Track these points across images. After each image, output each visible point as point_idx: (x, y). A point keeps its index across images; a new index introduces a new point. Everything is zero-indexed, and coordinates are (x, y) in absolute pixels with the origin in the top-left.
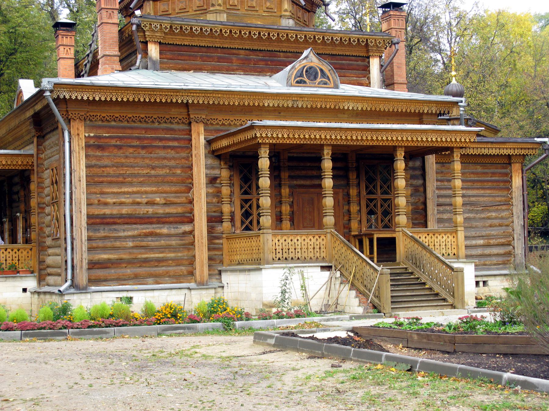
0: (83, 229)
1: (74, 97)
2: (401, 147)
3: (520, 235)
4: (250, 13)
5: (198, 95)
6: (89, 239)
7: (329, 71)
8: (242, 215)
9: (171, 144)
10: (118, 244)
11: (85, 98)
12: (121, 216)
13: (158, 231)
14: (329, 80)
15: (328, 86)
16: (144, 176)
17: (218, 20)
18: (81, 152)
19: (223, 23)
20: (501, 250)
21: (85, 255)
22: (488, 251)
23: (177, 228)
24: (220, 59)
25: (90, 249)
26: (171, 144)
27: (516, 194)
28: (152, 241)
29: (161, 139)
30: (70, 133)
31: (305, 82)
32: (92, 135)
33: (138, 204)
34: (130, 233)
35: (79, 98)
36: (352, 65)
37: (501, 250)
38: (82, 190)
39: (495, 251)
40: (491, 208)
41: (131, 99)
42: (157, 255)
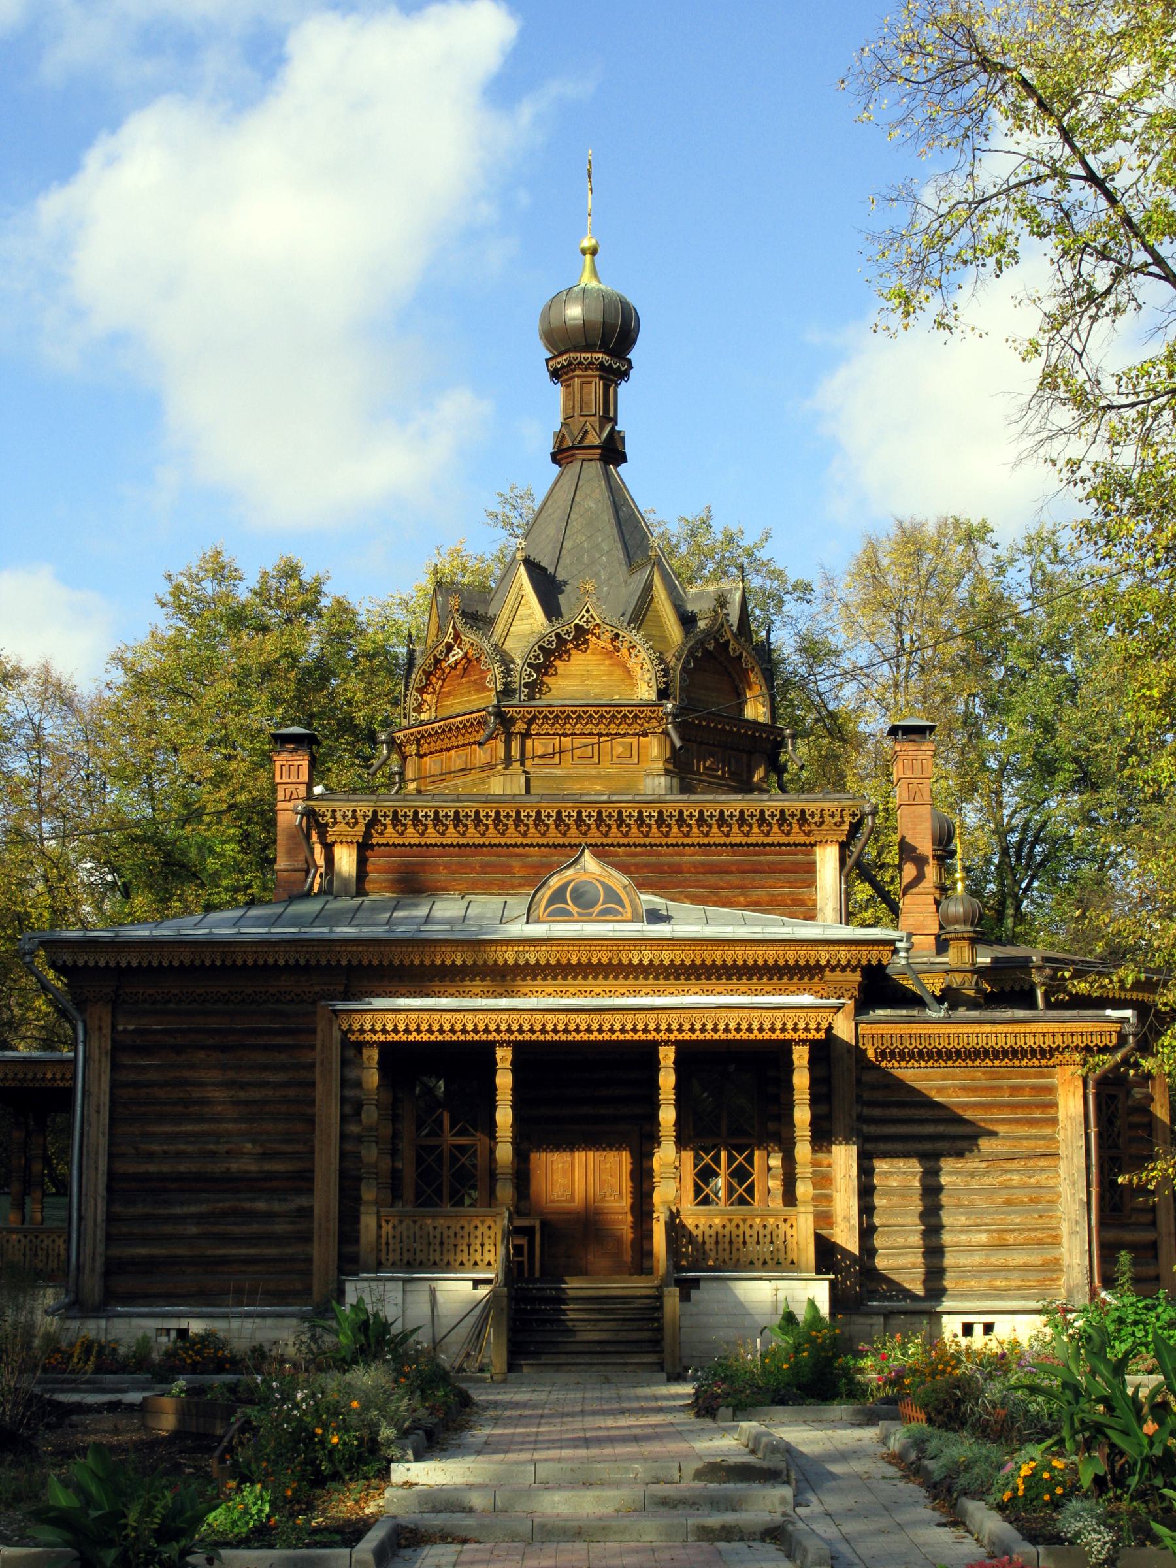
0: (99, 1199)
1: (81, 963)
2: (667, 1043)
3: (1077, 1222)
4: (581, 769)
5: (315, 949)
6: (111, 1218)
7: (625, 887)
8: (696, 1175)
9: (279, 1040)
10: (168, 1229)
11: (102, 963)
12: (180, 1177)
13: (247, 1205)
14: (623, 907)
15: (619, 918)
16: (225, 1103)
17: (508, 792)
18: (103, 1059)
19: (517, 798)
20: (1035, 1258)
21: (101, 1248)
22: (998, 1259)
23: (285, 1200)
24: (485, 868)
25: (109, 1238)
26: (279, 1040)
27: (1069, 1133)
28: (236, 1224)
29: (258, 1032)
30: (84, 1022)
31: (569, 913)
32: (131, 1027)
33: (213, 1154)
34: (193, 1209)
35: (91, 963)
36: (781, 862)
37: (1035, 1258)
38: (101, 1129)
39: (1019, 1258)
40: (1008, 1165)
41: (134, 963)
42: (244, 1251)
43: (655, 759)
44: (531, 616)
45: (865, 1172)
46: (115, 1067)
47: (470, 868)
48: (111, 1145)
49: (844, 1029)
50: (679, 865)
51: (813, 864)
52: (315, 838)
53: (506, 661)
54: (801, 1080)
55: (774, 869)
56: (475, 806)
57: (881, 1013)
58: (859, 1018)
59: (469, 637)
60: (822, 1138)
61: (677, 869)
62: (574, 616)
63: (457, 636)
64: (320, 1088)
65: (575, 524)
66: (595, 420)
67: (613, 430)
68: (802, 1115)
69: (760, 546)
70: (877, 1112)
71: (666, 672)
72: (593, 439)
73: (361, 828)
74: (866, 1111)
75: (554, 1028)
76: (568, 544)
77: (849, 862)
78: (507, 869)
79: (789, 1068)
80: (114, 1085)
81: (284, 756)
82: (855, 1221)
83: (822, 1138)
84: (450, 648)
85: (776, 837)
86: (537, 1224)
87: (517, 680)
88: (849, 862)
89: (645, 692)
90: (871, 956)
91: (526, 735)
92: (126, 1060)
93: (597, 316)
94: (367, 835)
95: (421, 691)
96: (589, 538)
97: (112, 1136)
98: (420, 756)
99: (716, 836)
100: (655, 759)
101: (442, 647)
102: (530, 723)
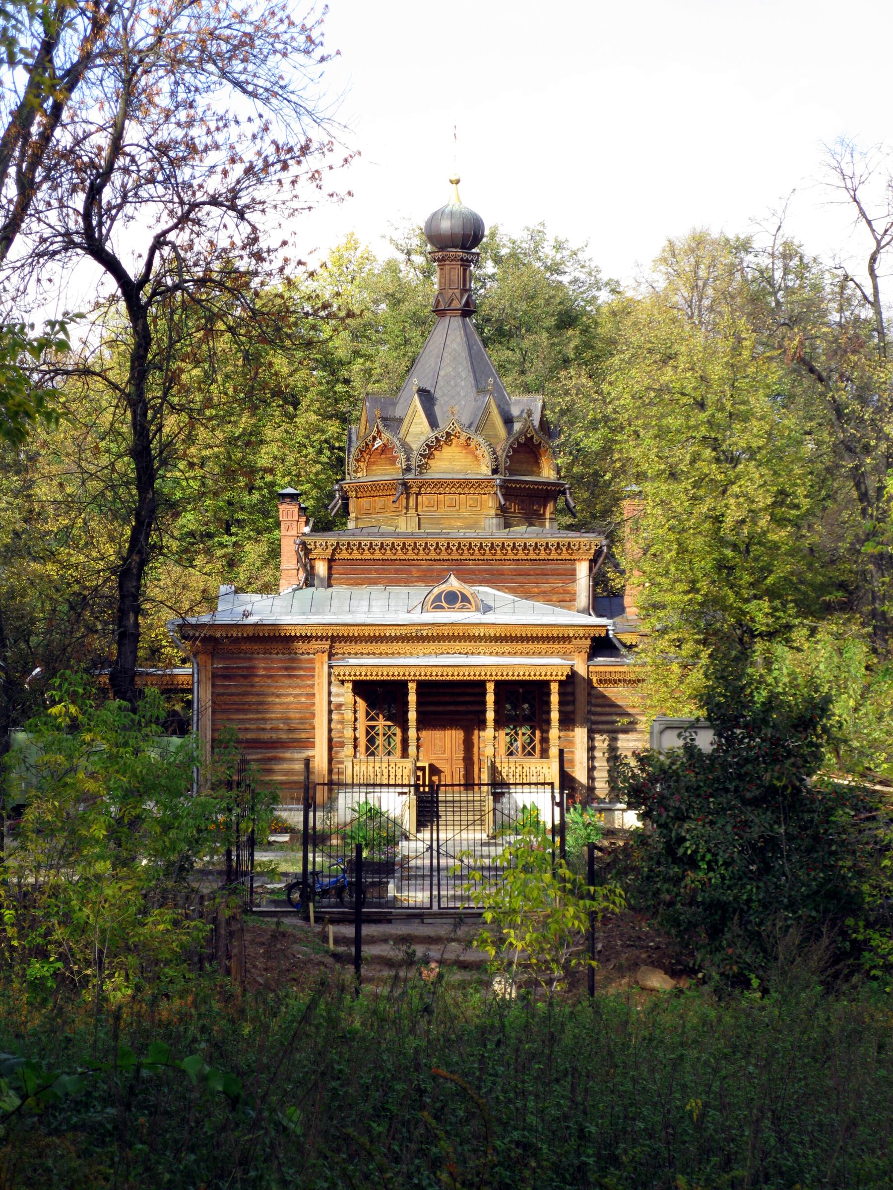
24: (397, 572)
31: (443, 608)
43: (491, 508)
44: (421, 424)
45: (591, 739)
46: (213, 686)
47: (389, 572)
48: (213, 724)
49: (581, 670)
50: (502, 570)
51: (575, 570)
52: (20, 144)
53: (407, 450)
54: (555, 699)
55: (554, 573)
56: (393, 540)
57: (600, 659)
58: (590, 663)
59: (386, 435)
60: (567, 722)
61: (501, 573)
62: (445, 426)
63: (379, 432)
64: (317, 696)
65: (447, 360)
66: (458, 292)
67: (469, 297)
68: (555, 715)
69: (581, 249)
70: (599, 709)
71: (496, 459)
72: (456, 304)
73: (330, 551)
74: (593, 709)
75: (436, 675)
76: (442, 373)
77: (595, 570)
78: (409, 572)
79: (549, 694)
80: (213, 693)
81: (284, 505)
82: (586, 765)
83: (567, 722)
84: (374, 438)
85: (554, 556)
86: (427, 766)
87: (413, 463)
88: (595, 570)
89: (485, 470)
90: (597, 632)
91: (418, 494)
92: (218, 682)
93: (459, 230)
94: (333, 554)
95: (358, 461)
96: (454, 369)
97: (213, 721)
98: (356, 497)
99: (521, 555)
100: (491, 508)
101: (370, 438)
102: (420, 488)
